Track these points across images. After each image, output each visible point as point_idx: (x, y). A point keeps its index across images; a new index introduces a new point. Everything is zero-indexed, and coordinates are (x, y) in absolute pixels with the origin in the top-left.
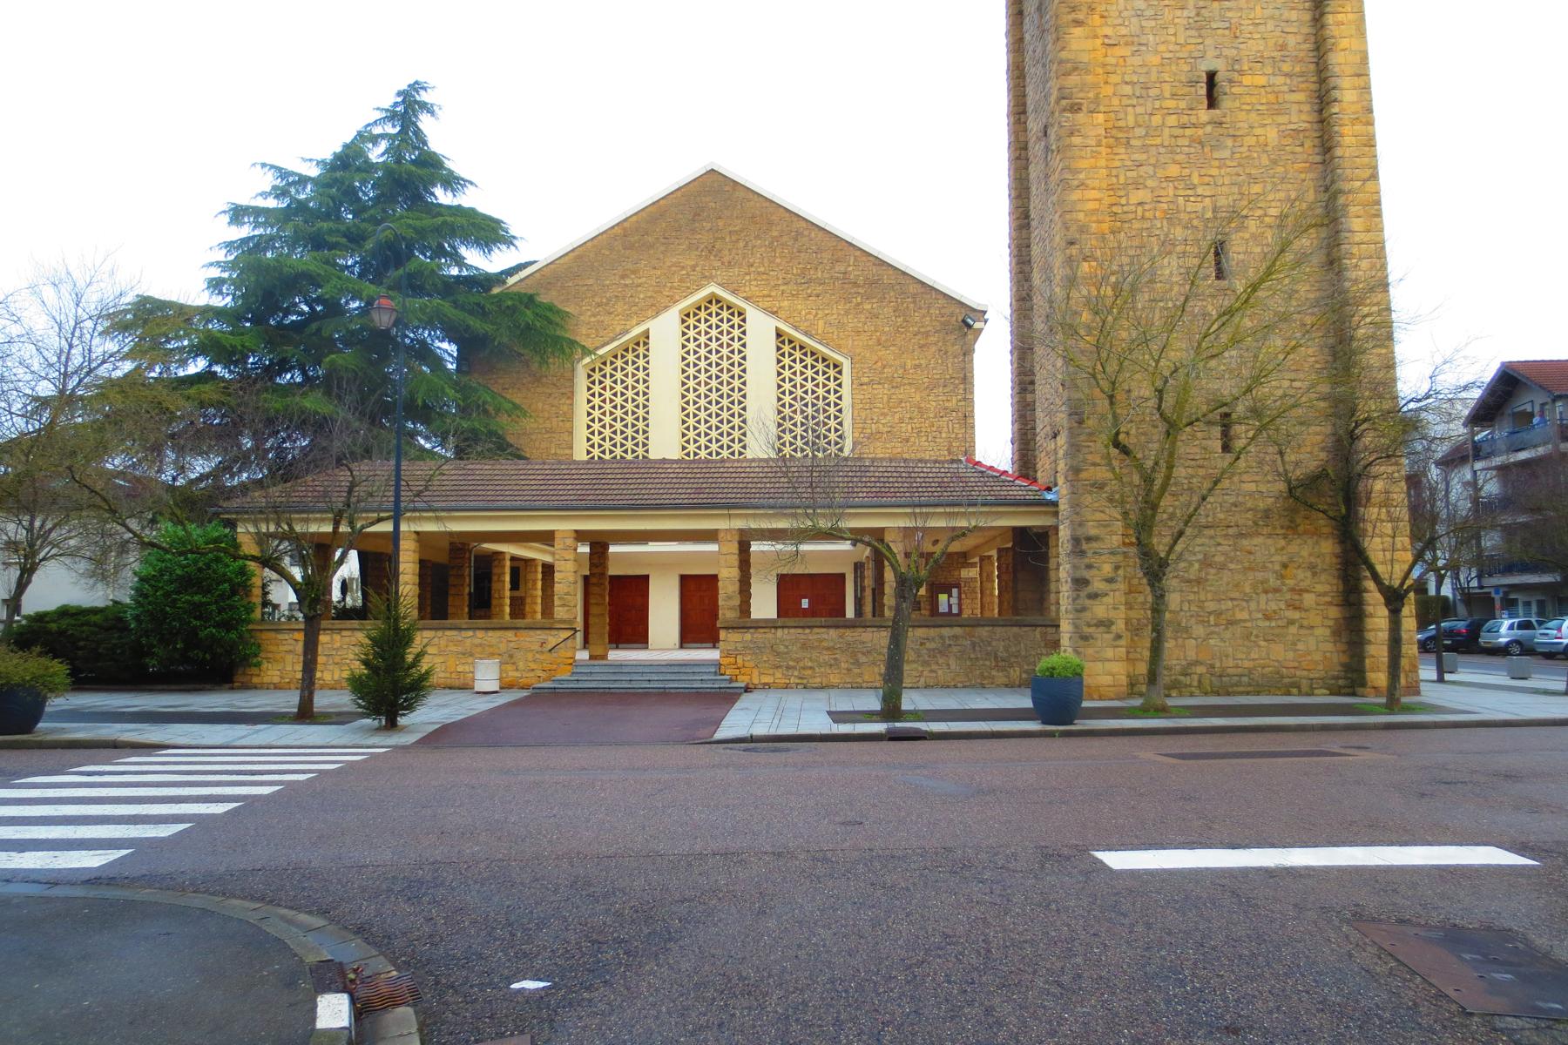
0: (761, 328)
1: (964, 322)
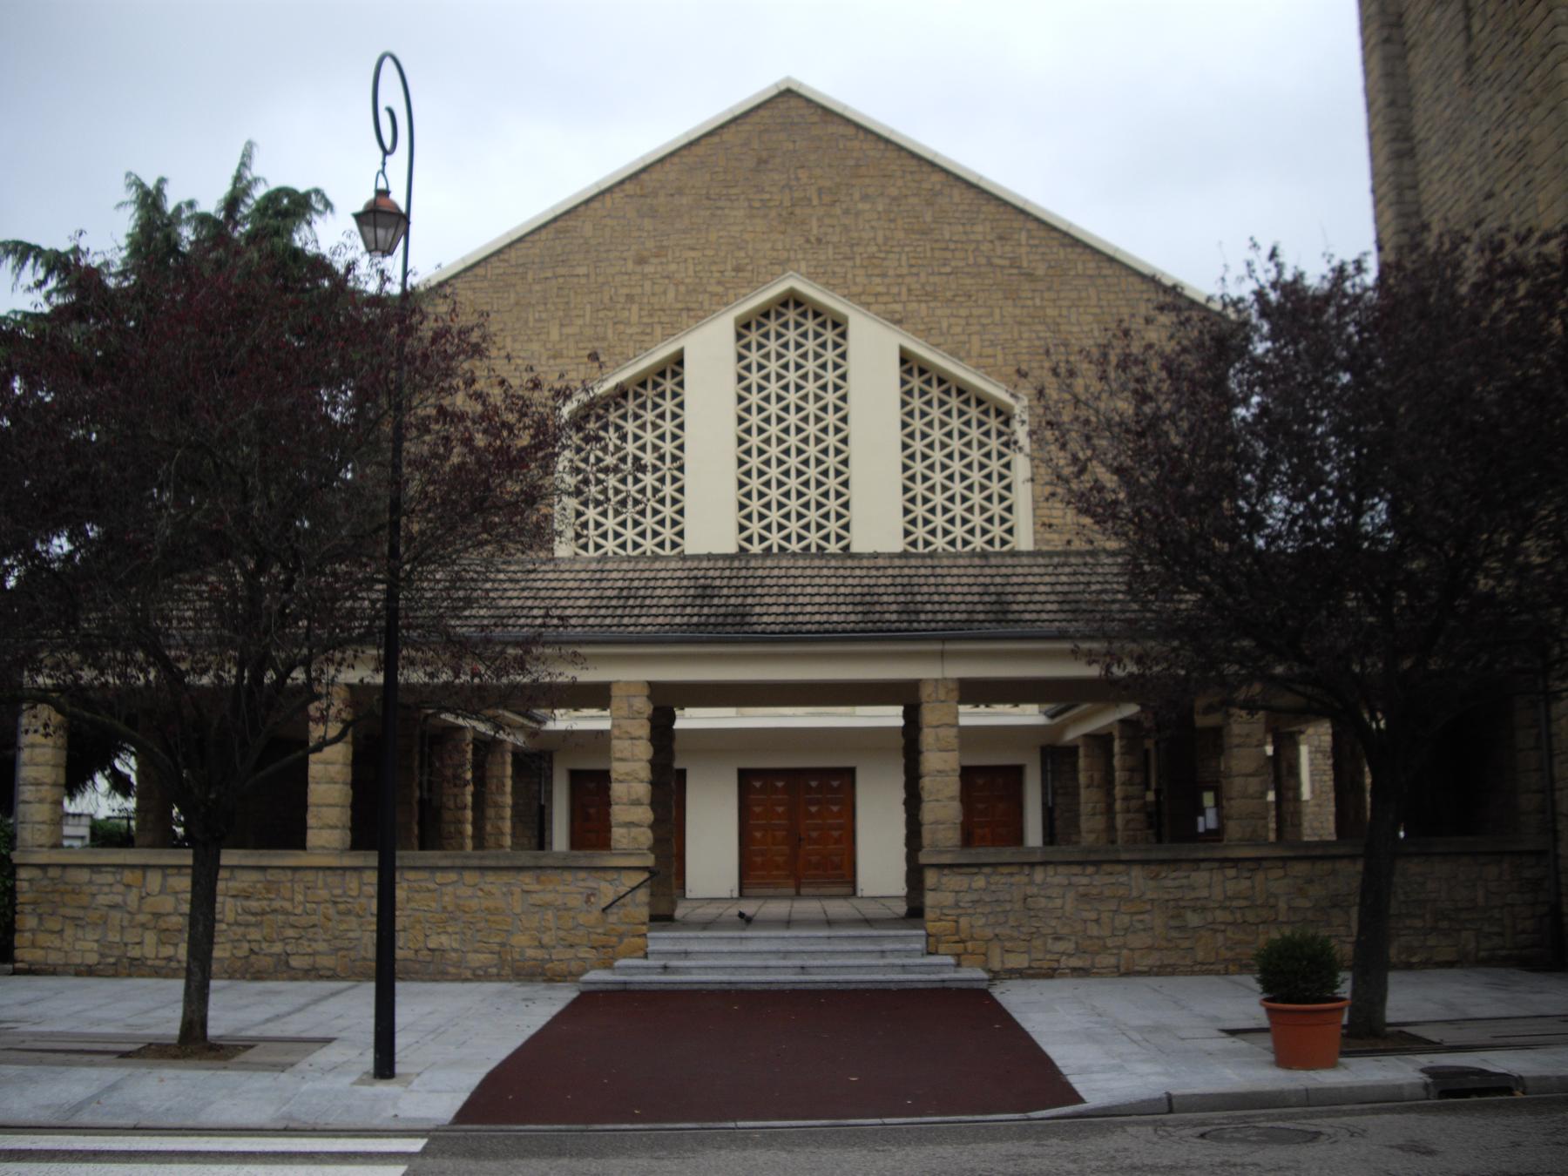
0: (874, 348)
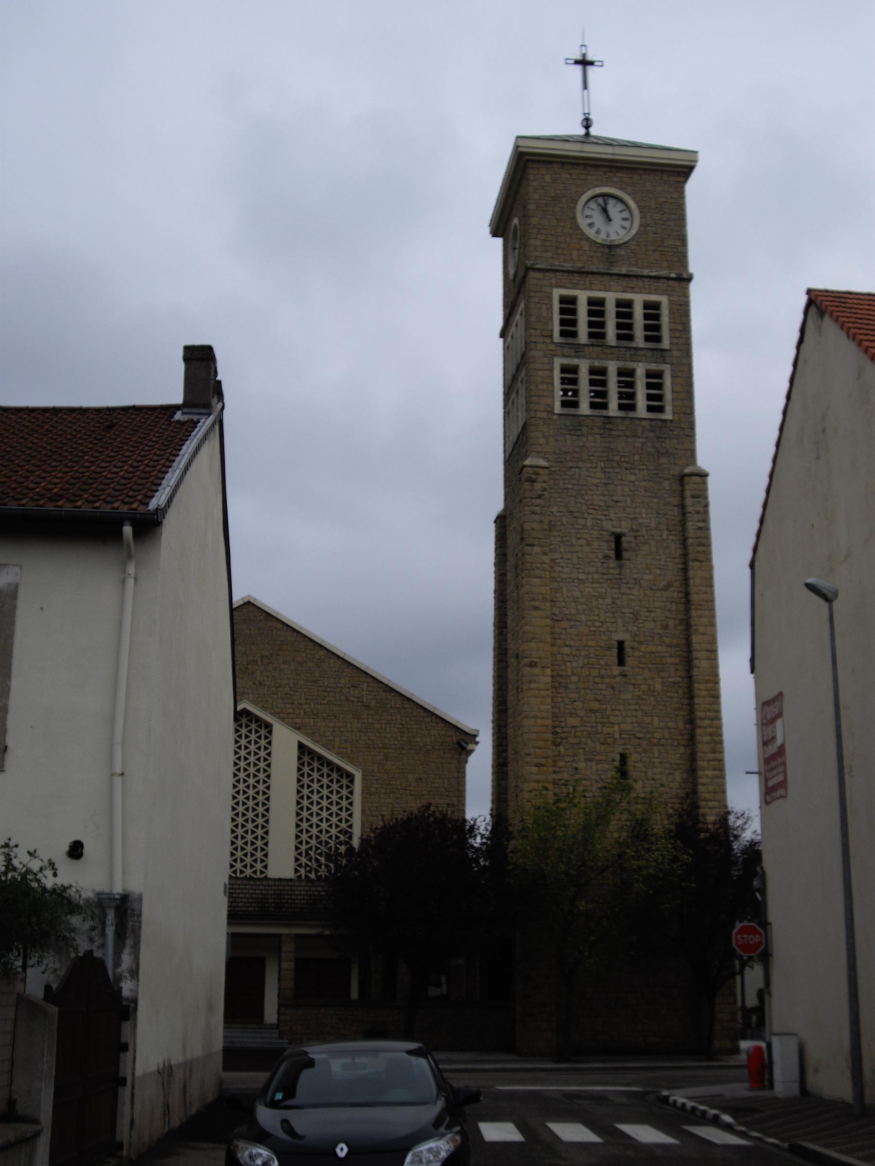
0: (285, 741)
1: (462, 742)
